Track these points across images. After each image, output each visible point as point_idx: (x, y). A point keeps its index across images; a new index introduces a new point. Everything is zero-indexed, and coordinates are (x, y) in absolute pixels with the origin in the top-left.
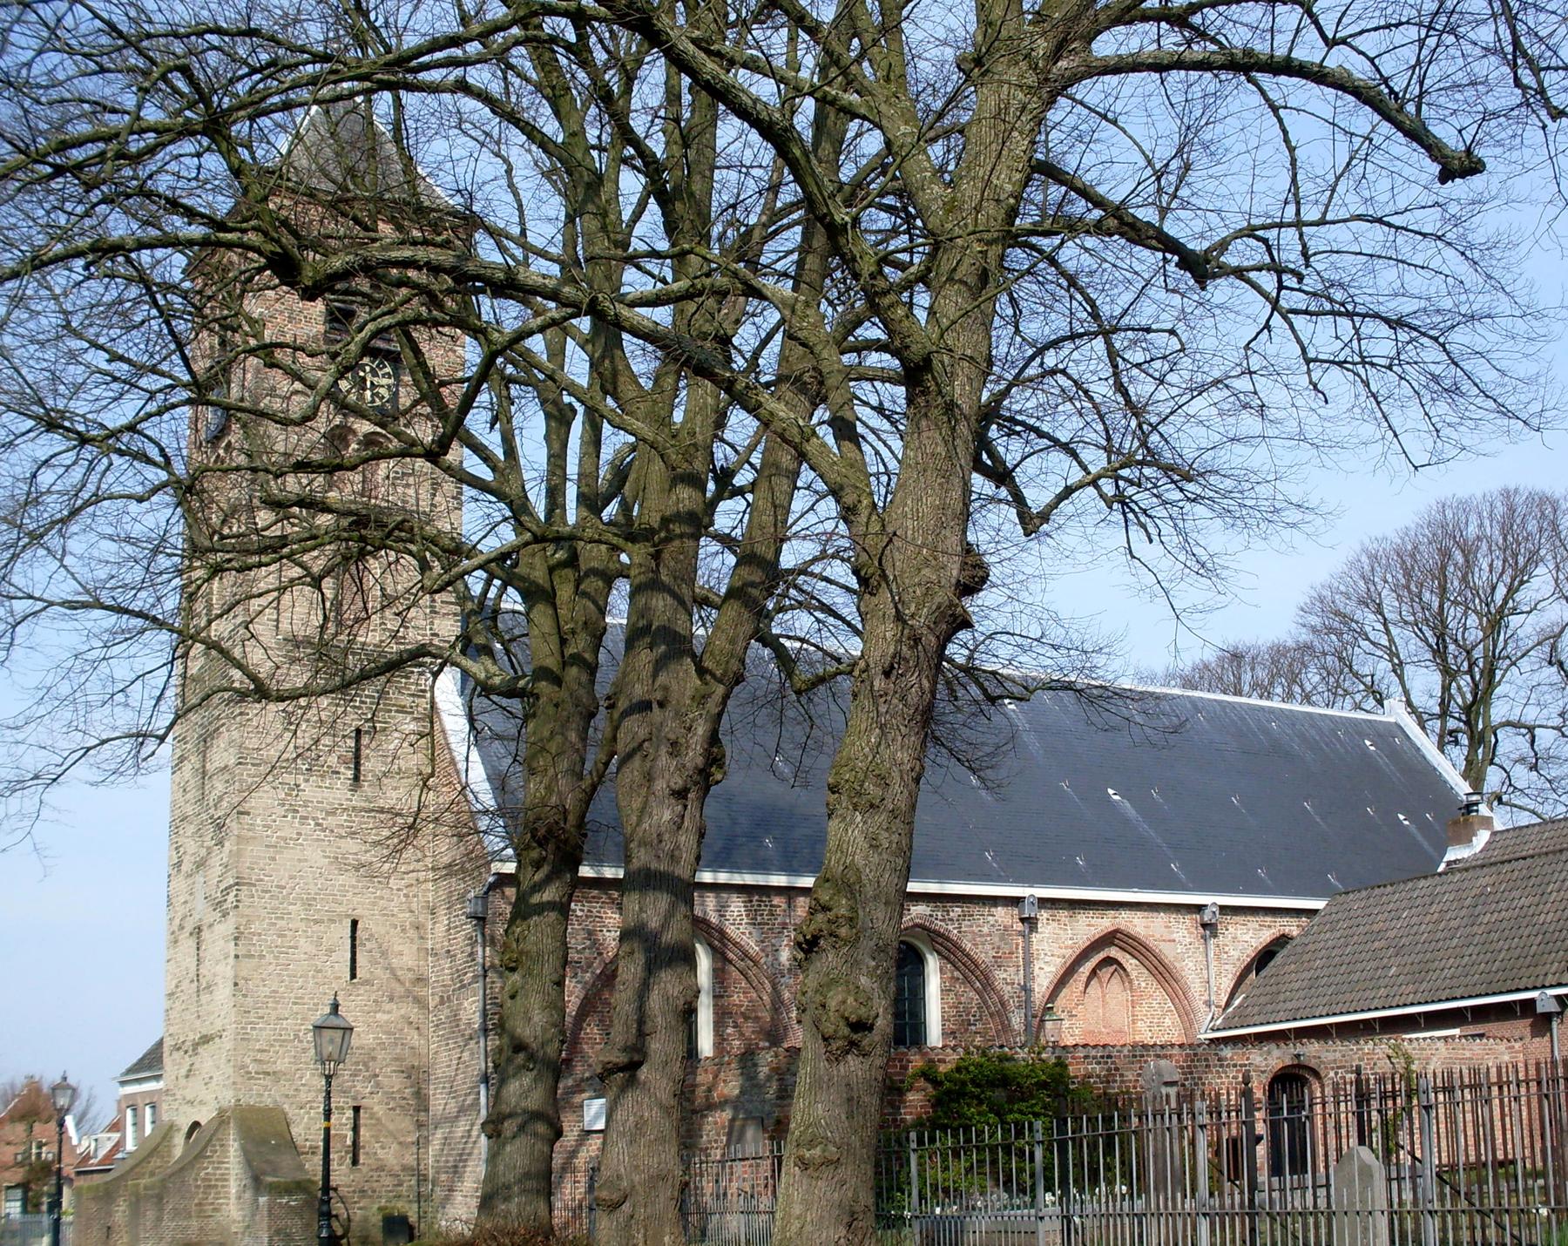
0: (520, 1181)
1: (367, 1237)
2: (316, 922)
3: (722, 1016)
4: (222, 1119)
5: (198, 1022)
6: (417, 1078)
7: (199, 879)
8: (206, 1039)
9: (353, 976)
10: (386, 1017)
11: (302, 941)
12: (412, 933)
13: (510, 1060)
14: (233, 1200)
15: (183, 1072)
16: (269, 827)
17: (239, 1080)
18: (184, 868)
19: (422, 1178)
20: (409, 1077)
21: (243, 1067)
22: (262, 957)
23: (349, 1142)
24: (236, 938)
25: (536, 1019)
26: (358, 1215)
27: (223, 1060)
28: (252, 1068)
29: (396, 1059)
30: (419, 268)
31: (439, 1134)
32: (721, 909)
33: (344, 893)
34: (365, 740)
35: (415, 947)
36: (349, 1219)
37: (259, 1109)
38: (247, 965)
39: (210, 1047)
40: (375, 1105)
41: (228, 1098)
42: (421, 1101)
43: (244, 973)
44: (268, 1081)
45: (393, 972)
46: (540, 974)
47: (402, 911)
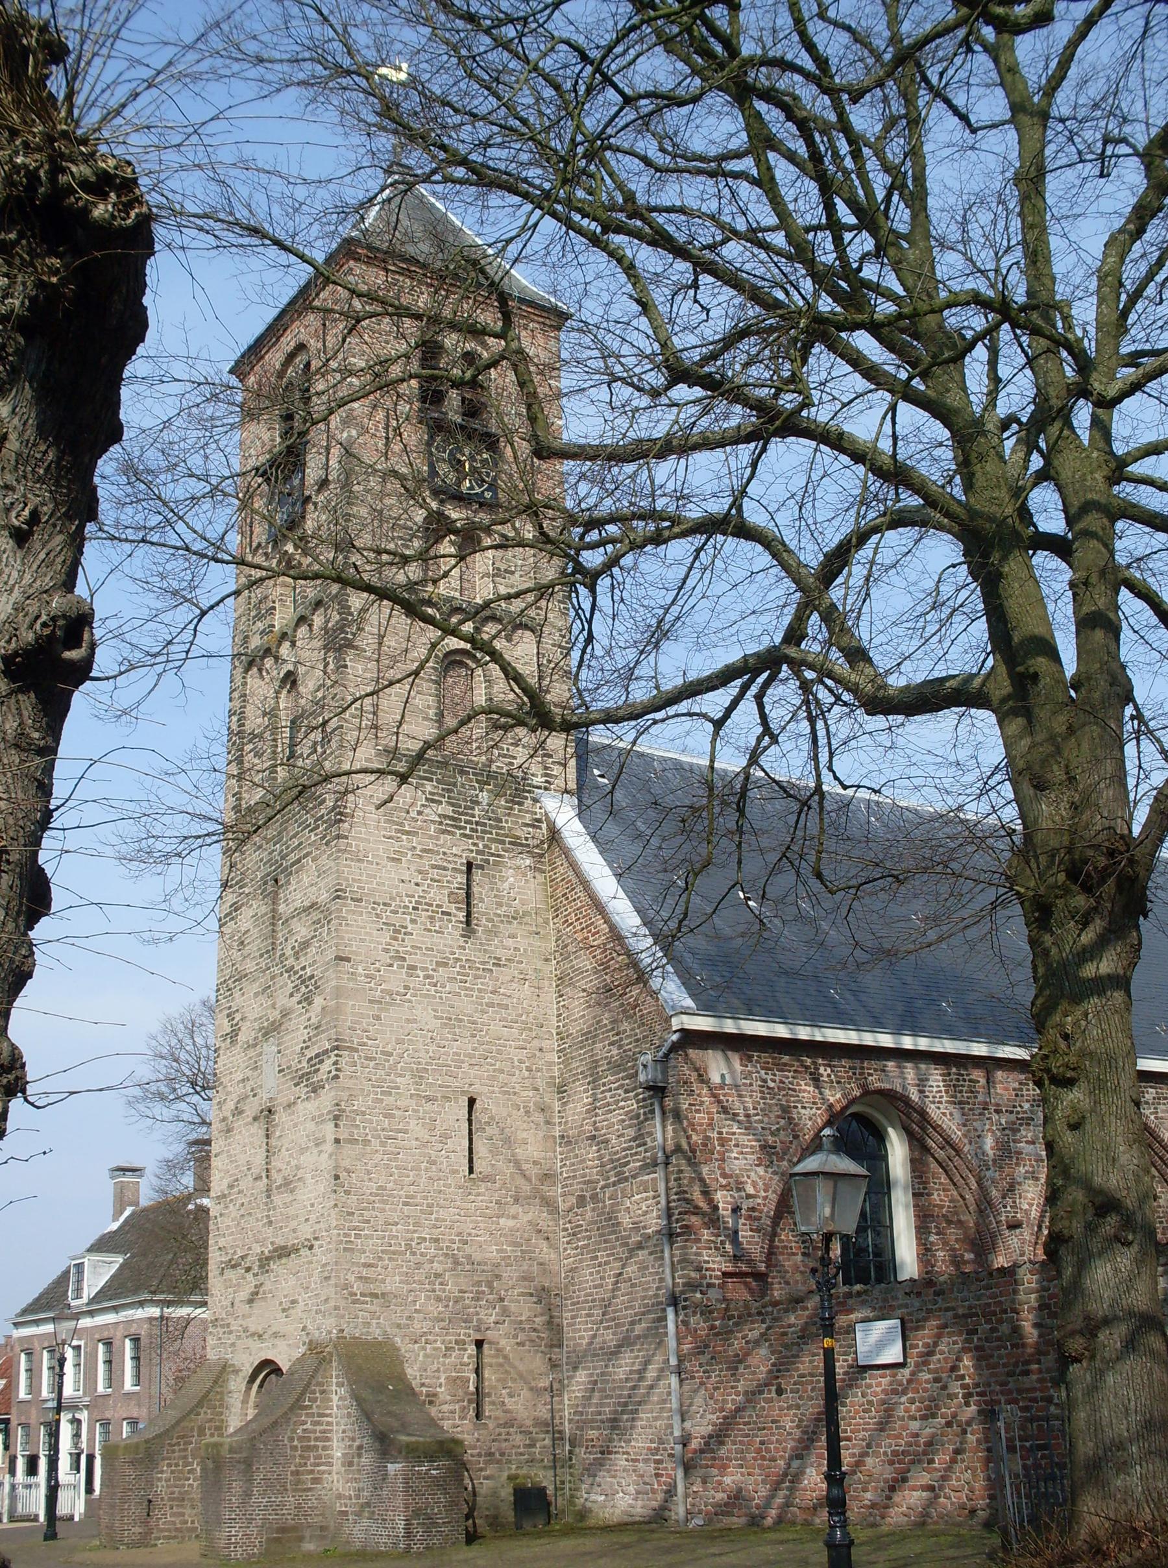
0: (1139, 1436)
1: (496, 1517)
2: (429, 1099)
3: (924, 1220)
4: (318, 1354)
5: (269, 1231)
6: (548, 1299)
7: (270, 1048)
8: (283, 1252)
9: (471, 1171)
10: (511, 1223)
11: (413, 1123)
12: (538, 1117)
13: (1091, 1228)
14: (337, 1466)
15: (244, 1294)
16: (372, 977)
17: (342, 1303)
18: (242, 1037)
19: (557, 1437)
20: (539, 1302)
21: (346, 1286)
22: (366, 1142)
23: (472, 1388)
24: (336, 1118)
25: (1124, 1159)
26: (485, 1487)
27: (316, 1277)
28: (357, 1287)
29: (524, 1279)
30: (790, 117)
31: (582, 1376)
32: (922, 1082)
33: (459, 1064)
34: (477, 875)
35: (541, 1134)
36: (474, 1494)
37: (367, 1342)
38: (347, 1150)
39: (292, 1262)
40: (502, 1338)
41: (325, 1327)
42: (554, 1333)
43: (346, 1163)
44: (374, 1306)
45: (517, 1163)
46: (1116, 1089)
47: (525, 1088)
